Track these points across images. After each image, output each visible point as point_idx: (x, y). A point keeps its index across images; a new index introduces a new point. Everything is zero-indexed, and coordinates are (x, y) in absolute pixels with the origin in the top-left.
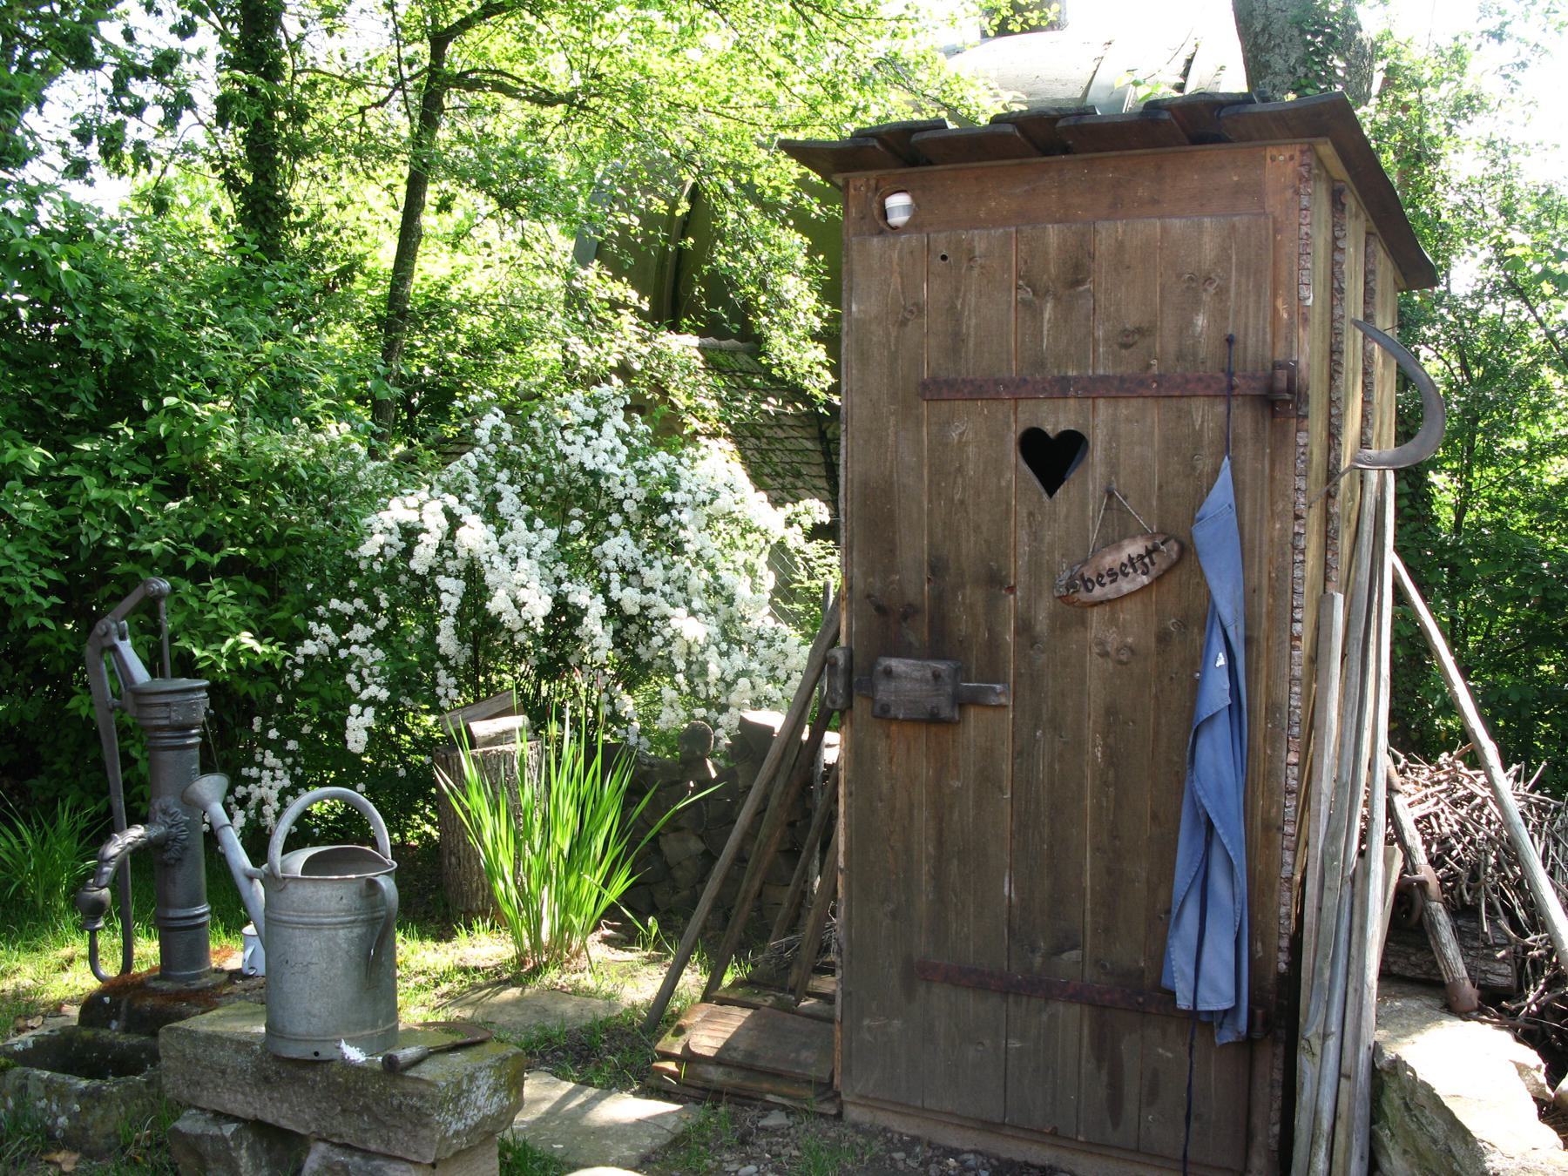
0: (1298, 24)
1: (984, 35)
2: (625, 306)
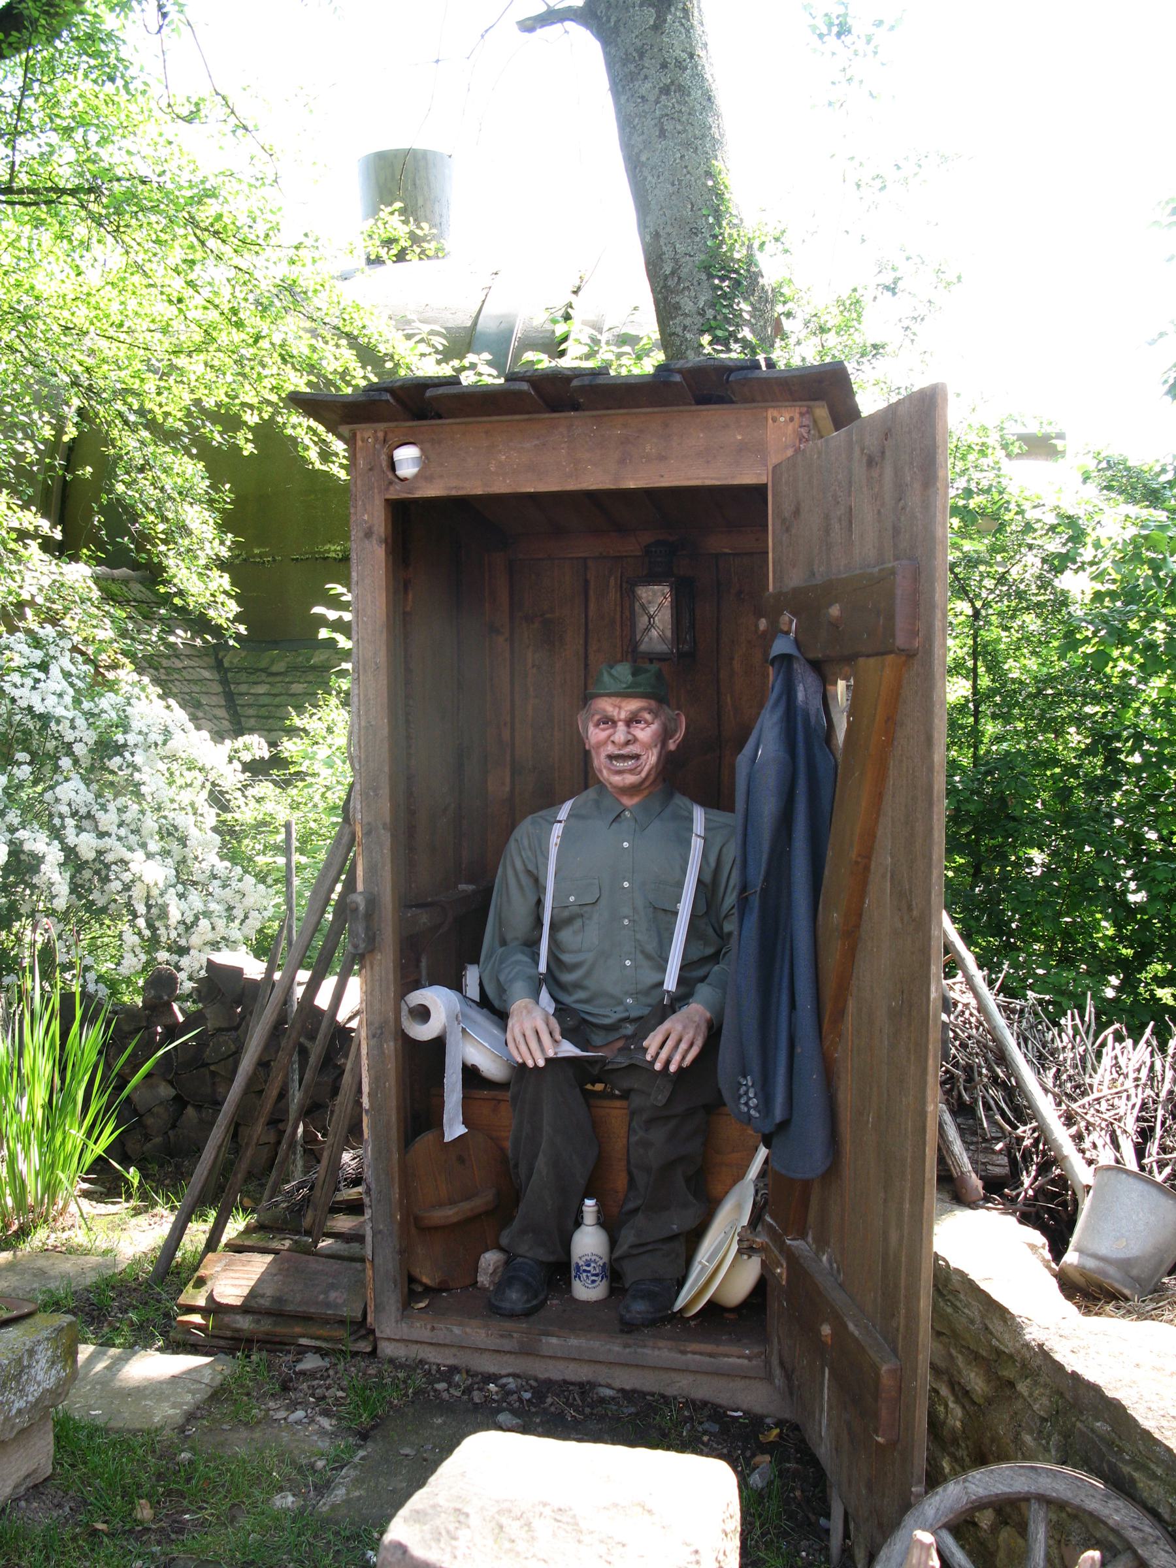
0: (707, 269)
2: (35, 536)
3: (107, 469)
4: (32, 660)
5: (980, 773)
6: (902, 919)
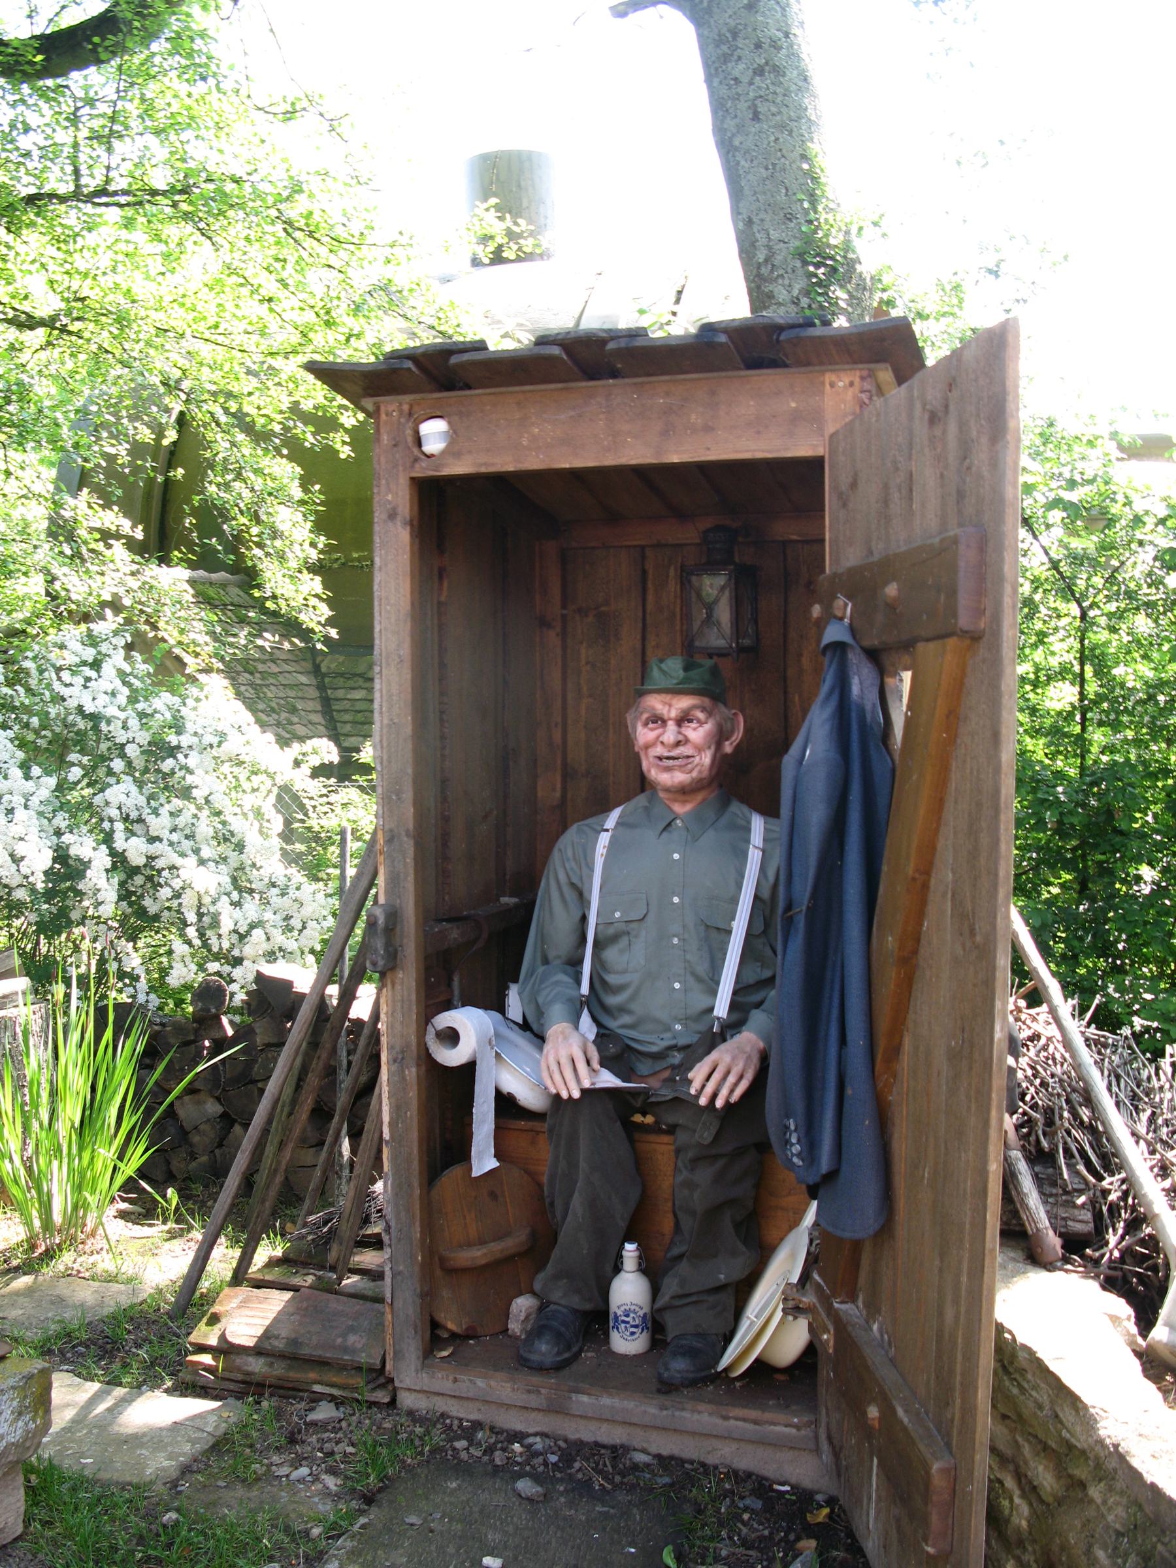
0: (801, 255)
1: (476, 262)
2: (118, 536)
3: (200, 470)
5: (1084, 784)
6: (963, 945)
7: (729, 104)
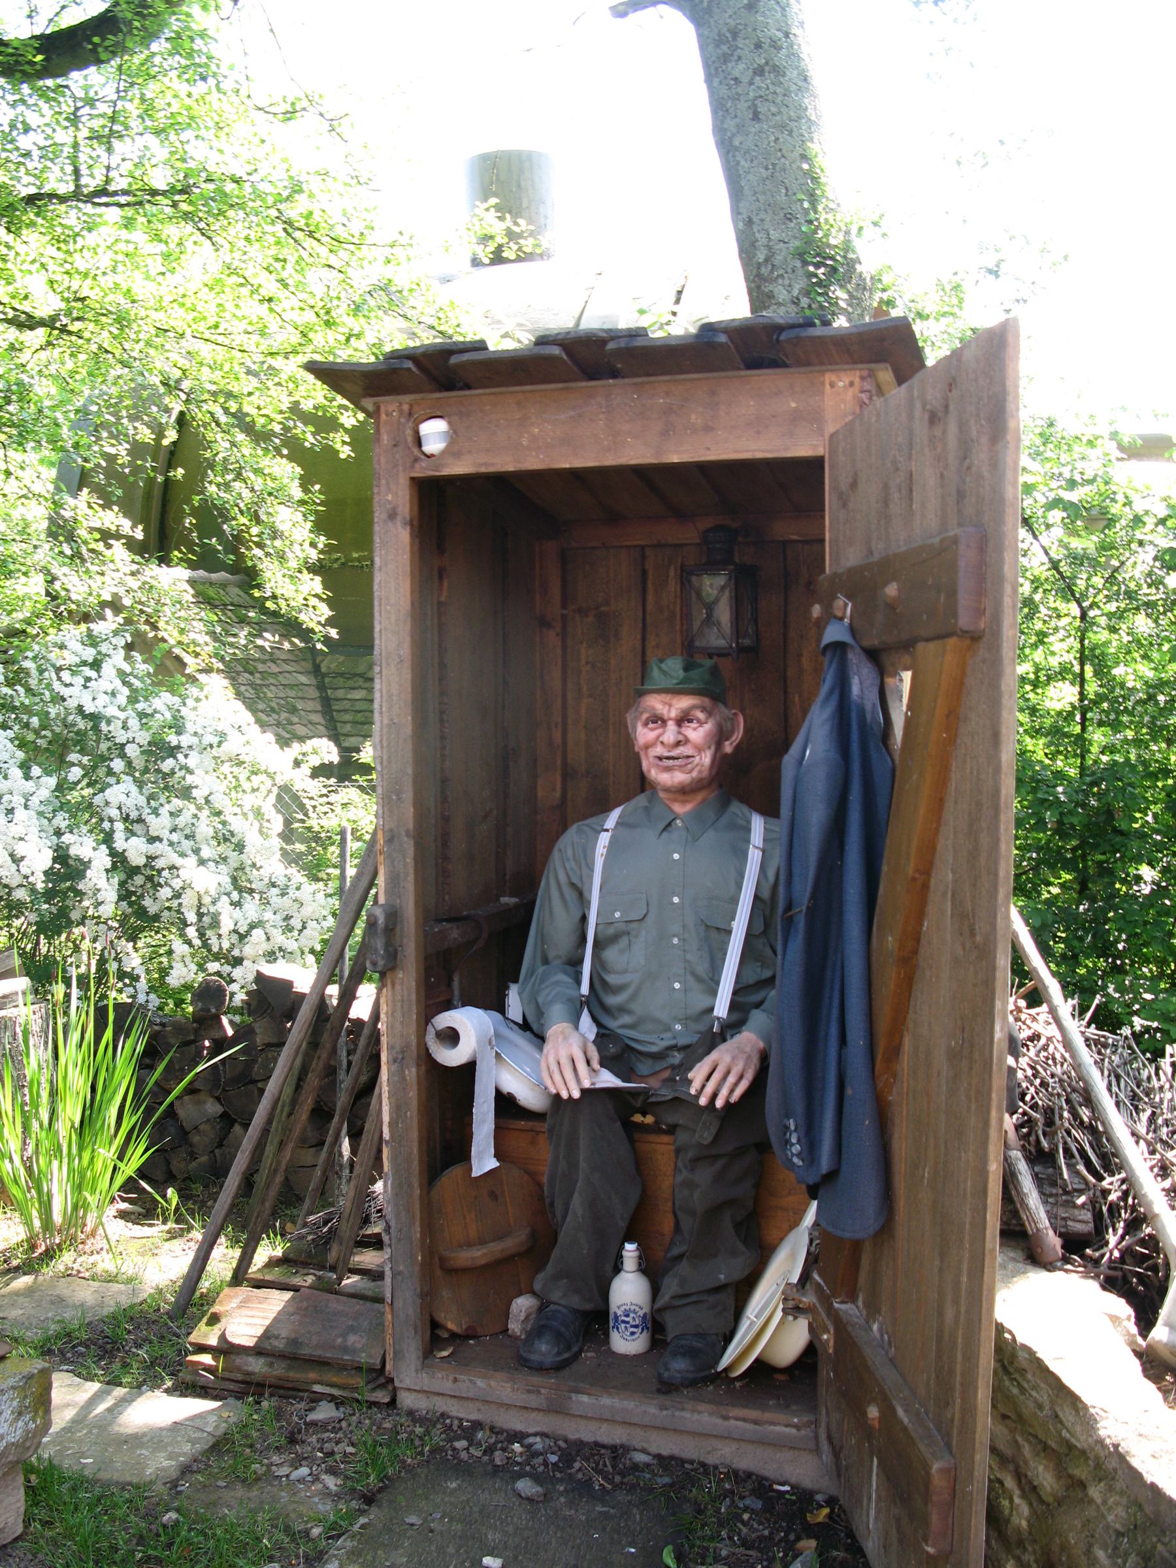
0: (801, 255)
1: (476, 262)
2: (118, 536)
3: (200, 470)
4: (84, 658)
5: (1084, 784)
6: (963, 945)
7: (729, 104)
